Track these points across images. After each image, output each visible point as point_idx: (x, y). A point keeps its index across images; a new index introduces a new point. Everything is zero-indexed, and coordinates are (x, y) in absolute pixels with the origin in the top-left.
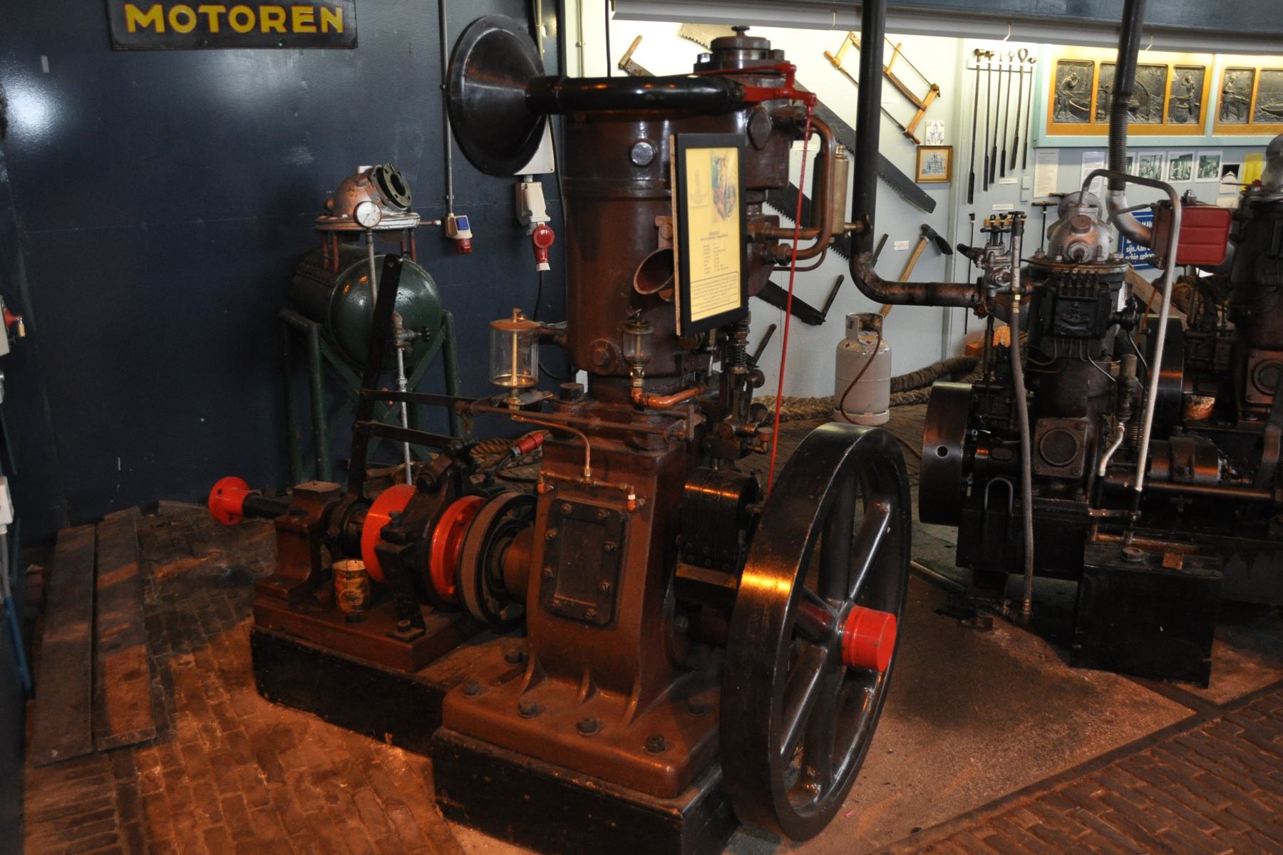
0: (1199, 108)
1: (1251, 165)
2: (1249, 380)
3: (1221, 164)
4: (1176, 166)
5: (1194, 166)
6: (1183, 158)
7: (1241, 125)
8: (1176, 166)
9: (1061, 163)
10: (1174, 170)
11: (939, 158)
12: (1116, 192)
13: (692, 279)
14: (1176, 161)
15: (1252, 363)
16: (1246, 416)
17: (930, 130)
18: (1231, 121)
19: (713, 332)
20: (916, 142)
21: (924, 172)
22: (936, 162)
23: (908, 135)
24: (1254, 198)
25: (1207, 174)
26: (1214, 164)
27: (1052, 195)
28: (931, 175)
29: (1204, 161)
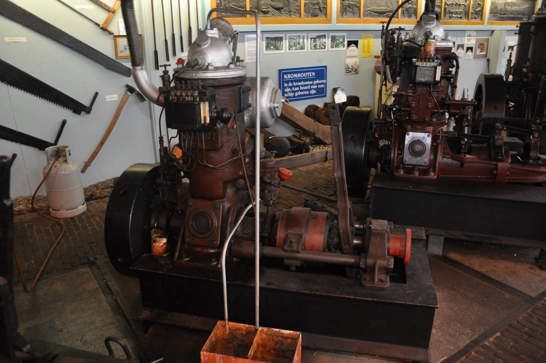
0: (326, 8)
1: (366, 41)
4: (315, 41)
5: (328, 41)
6: (319, 37)
7: (356, 19)
8: (315, 41)
10: (313, 44)
12: (139, 68)
13: (15, 129)
14: (315, 38)
18: (349, 17)
19: (415, 7)
20: (111, 33)
21: (122, 52)
23: (104, 29)
25: (337, 46)
26: (341, 40)
29: (333, 38)
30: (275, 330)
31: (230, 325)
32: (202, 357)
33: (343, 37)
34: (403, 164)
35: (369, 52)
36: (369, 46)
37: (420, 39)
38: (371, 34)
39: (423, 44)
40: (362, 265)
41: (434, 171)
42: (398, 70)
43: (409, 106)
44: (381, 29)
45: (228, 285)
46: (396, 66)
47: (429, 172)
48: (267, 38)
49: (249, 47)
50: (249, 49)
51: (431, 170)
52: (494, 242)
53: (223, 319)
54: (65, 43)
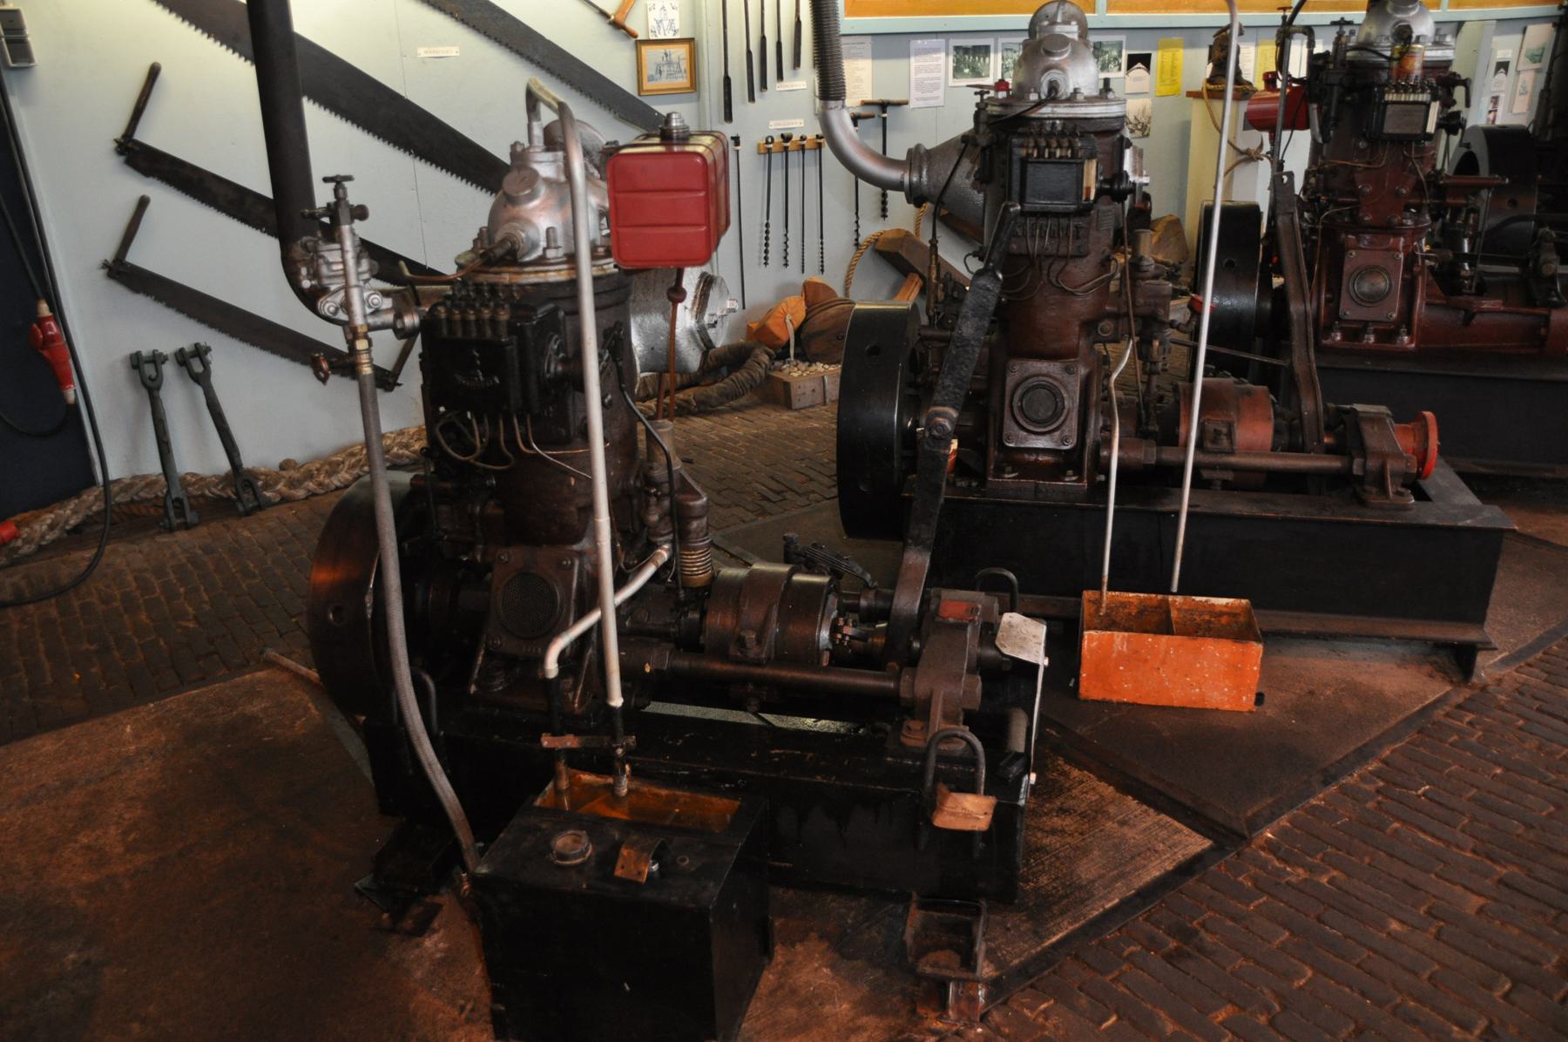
2: (1007, 414)
3: (1125, 54)
9: (876, 56)
11: (674, 57)
12: (832, 103)
15: (1010, 381)
16: (999, 471)
17: (653, 16)
20: (631, 35)
21: (651, 79)
22: (669, 63)
23: (617, 25)
24: (994, 110)
26: (1115, 53)
27: (865, 104)
28: (664, 82)
30: (1198, 599)
31: (1107, 595)
32: (1085, 643)
33: (1119, 45)
34: (1339, 319)
35: (1174, 82)
36: (1173, 67)
37: (1386, 48)
38: (1176, 38)
39: (1396, 55)
40: (1357, 469)
41: (1409, 333)
42: (1333, 114)
43: (1355, 193)
44: (1279, 22)
45: (1116, 511)
46: (1329, 104)
47: (1398, 334)
48: (957, 48)
49: (918, 70)
50: (920, 76)
51: (1403, 330)
52: (1548, 475)
53: (1098, 587)
54: (536, 57)
